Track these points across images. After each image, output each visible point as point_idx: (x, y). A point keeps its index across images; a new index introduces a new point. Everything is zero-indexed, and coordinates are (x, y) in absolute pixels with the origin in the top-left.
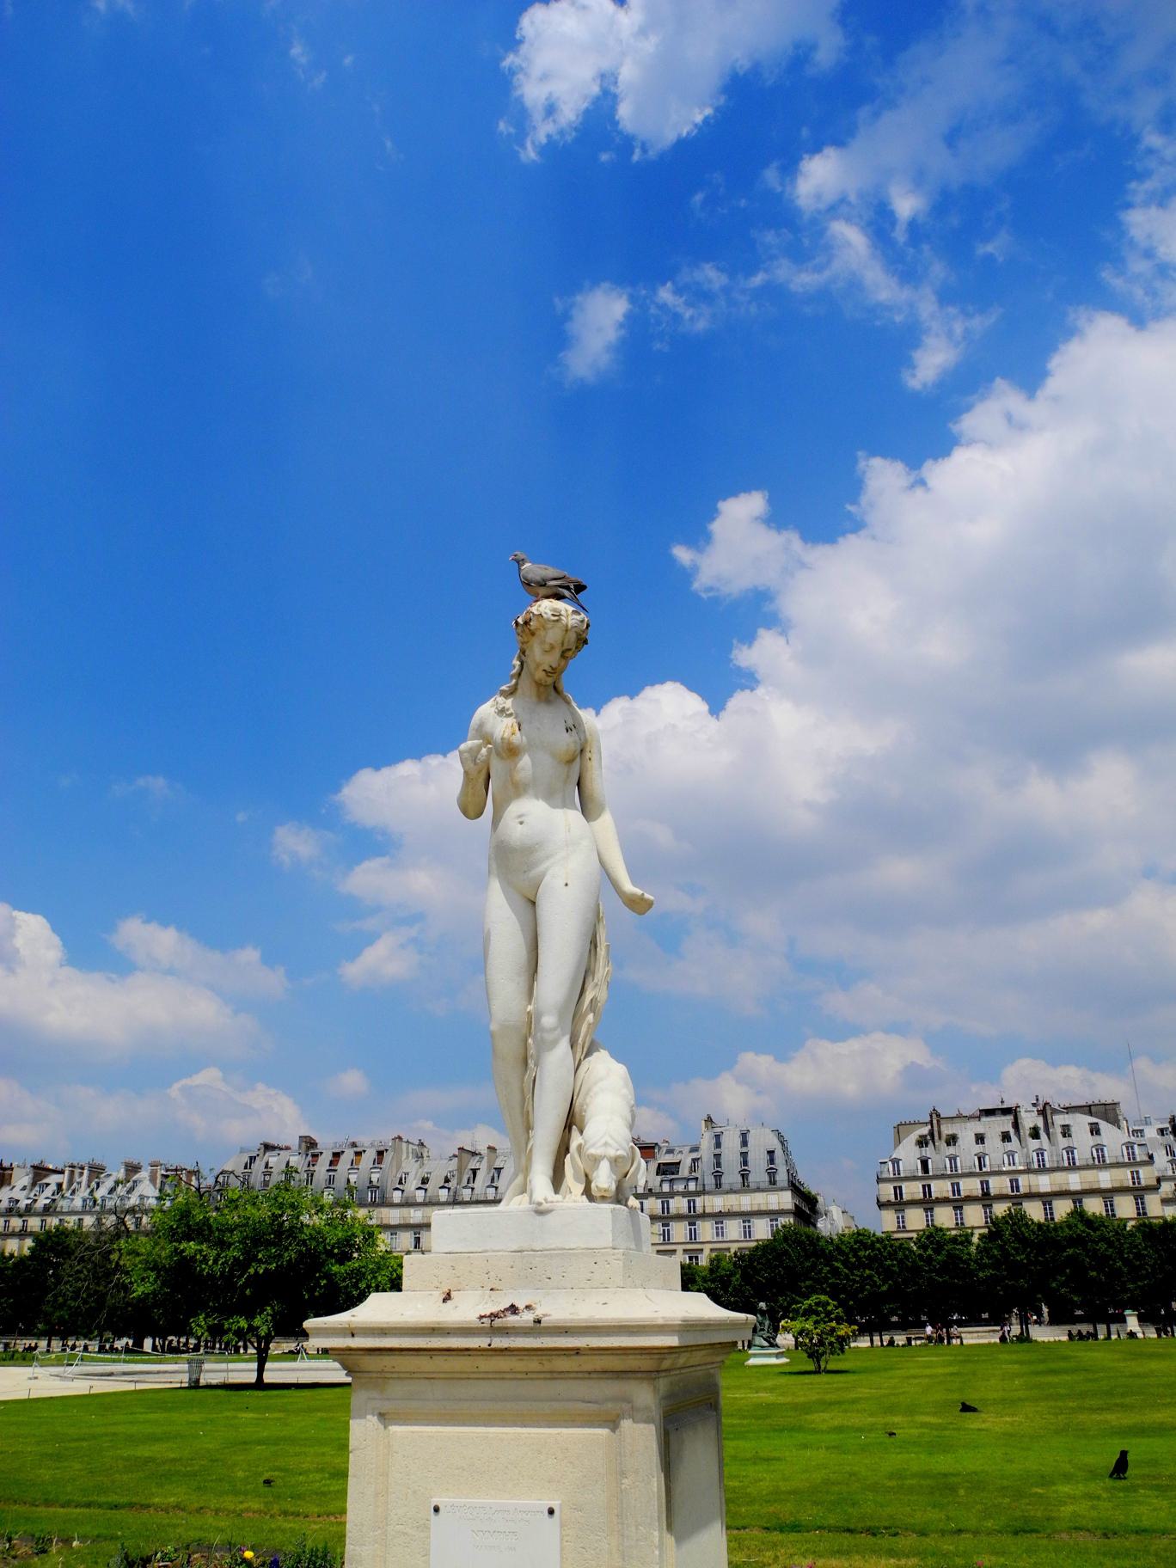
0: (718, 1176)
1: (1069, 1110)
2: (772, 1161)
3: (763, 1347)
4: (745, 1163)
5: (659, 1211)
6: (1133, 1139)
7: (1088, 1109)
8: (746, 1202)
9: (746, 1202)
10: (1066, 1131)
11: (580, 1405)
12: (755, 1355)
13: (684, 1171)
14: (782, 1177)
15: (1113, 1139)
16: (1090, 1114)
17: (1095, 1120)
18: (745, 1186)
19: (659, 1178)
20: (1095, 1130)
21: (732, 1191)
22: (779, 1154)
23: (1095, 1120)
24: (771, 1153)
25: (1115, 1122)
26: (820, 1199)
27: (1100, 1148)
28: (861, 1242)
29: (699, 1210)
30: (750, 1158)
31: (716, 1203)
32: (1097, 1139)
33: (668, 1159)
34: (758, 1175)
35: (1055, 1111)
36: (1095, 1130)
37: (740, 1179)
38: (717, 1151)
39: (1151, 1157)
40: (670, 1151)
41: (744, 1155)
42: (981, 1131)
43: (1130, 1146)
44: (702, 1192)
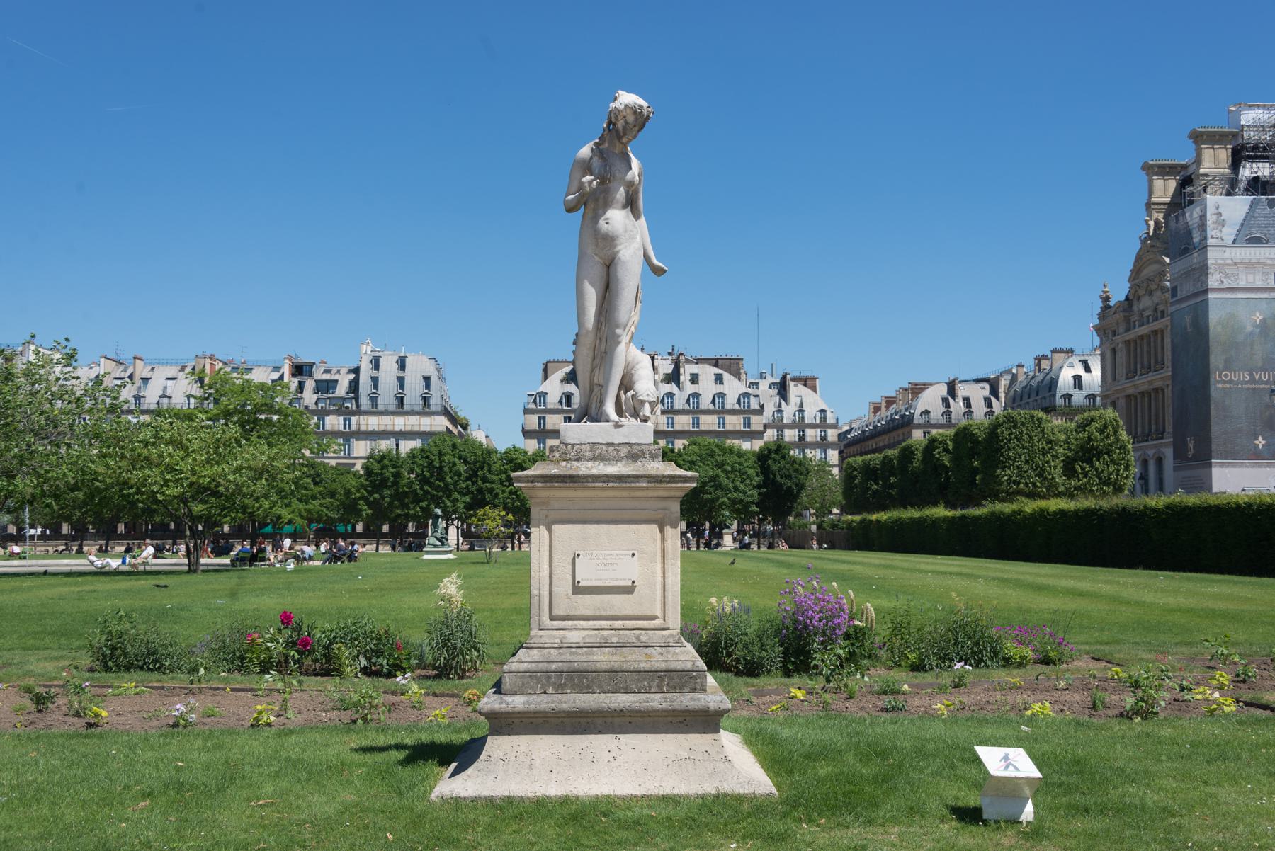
0: (374, 399)
1: (698, 361)
2: (428, 386)
3: (435, 546)
4: (402, 386)
5: (663, 427)
6: (749, 390)
7: (716, 363)
8: (400, 423)
9: (400, 423)
10: (694, 379)
11: (546, 593)
12: (428, 553)
13: (341, 390)
14: (435, 403)
15: (733, 388)
16: (716, 365)
17: (720, 371)
18: (375, 411)
19: (315, 396)
20: (719, 379)
21: (412, 413)
22: (434, 380)
23: (720, 371)
24: (427, 379)
25: (737, 374)
27: (722, 395)
28: (511, 461)
29: (353, 428)
30: (407, 381)
31: (372, 423)
32: (720, 389)
33: (326, 377)
34: (413, 400)
35: (688, 361)
36: (719, 379)
37: (422, 403)
38: (401, 373)
39: (762, 407)
40: (327, 371)
41: (401, 380)
42: (695, 371)
43: (747, 395)
44: (359, 412)
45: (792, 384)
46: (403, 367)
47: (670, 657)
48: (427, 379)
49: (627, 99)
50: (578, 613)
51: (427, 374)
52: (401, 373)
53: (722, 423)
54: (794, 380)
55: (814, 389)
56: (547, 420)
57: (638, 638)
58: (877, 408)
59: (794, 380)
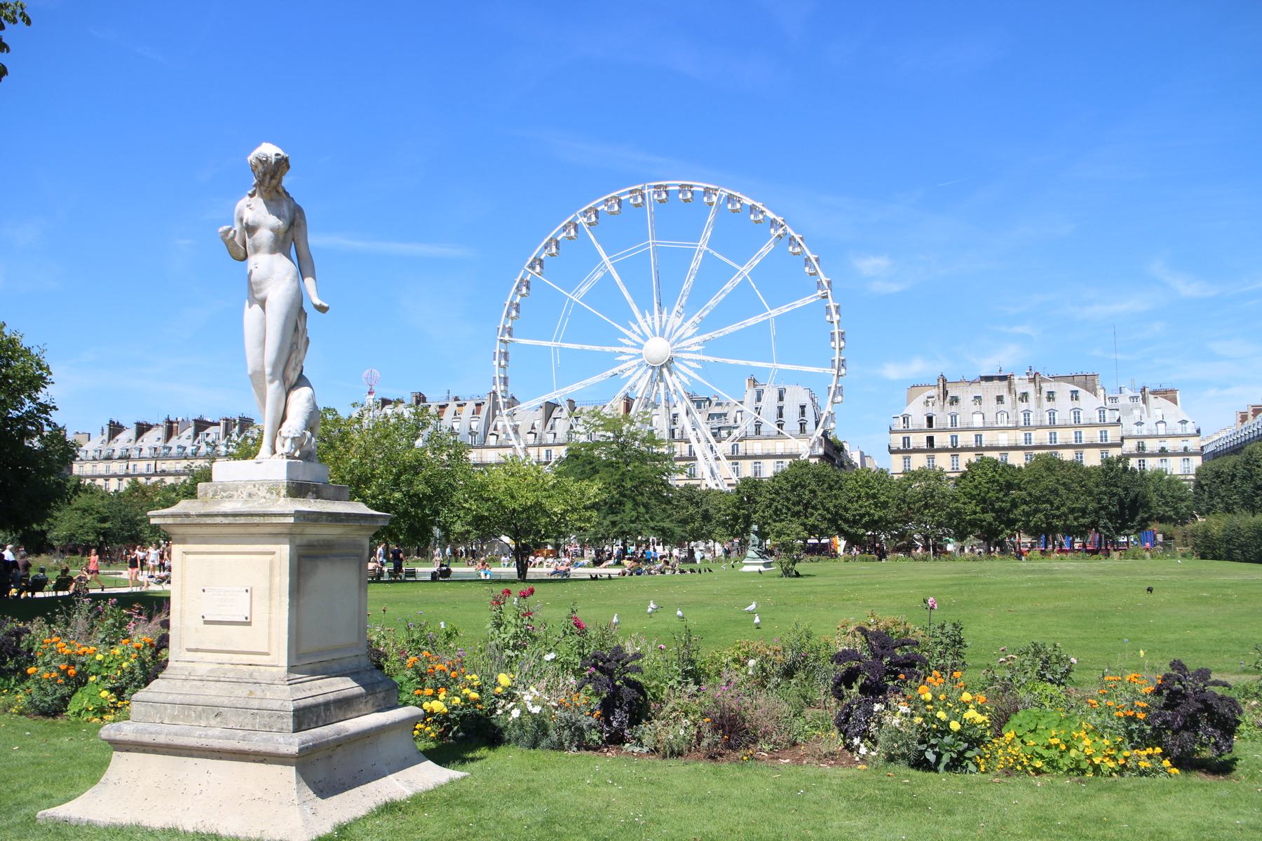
1: (1056, 378)
2: (803, 413)
7: (1070, 379)
15: (1089, 405)
16: (1073, 383)
17: (1076, 388)
21: (768, 438)
23: (1076, 388)
24: (803, 407)
25: (1094, 391)
26: (846, 446)
32: (1076, 404)
36: (1075, 395)
38: (781, 404)
45: (1151, 397)
46: (781, 399)
47: (268, 695)
48: (803, 407)
49: (269, 150)
50: (204, 647)
51: (803, 403)
52: (759, 404)
53: (1053, 437)
54: (1154, 393)
55: (1174, 401)
56: (1109, 434)
57: (251, 675)
58: (1244, 418)
59: (1154, 393)
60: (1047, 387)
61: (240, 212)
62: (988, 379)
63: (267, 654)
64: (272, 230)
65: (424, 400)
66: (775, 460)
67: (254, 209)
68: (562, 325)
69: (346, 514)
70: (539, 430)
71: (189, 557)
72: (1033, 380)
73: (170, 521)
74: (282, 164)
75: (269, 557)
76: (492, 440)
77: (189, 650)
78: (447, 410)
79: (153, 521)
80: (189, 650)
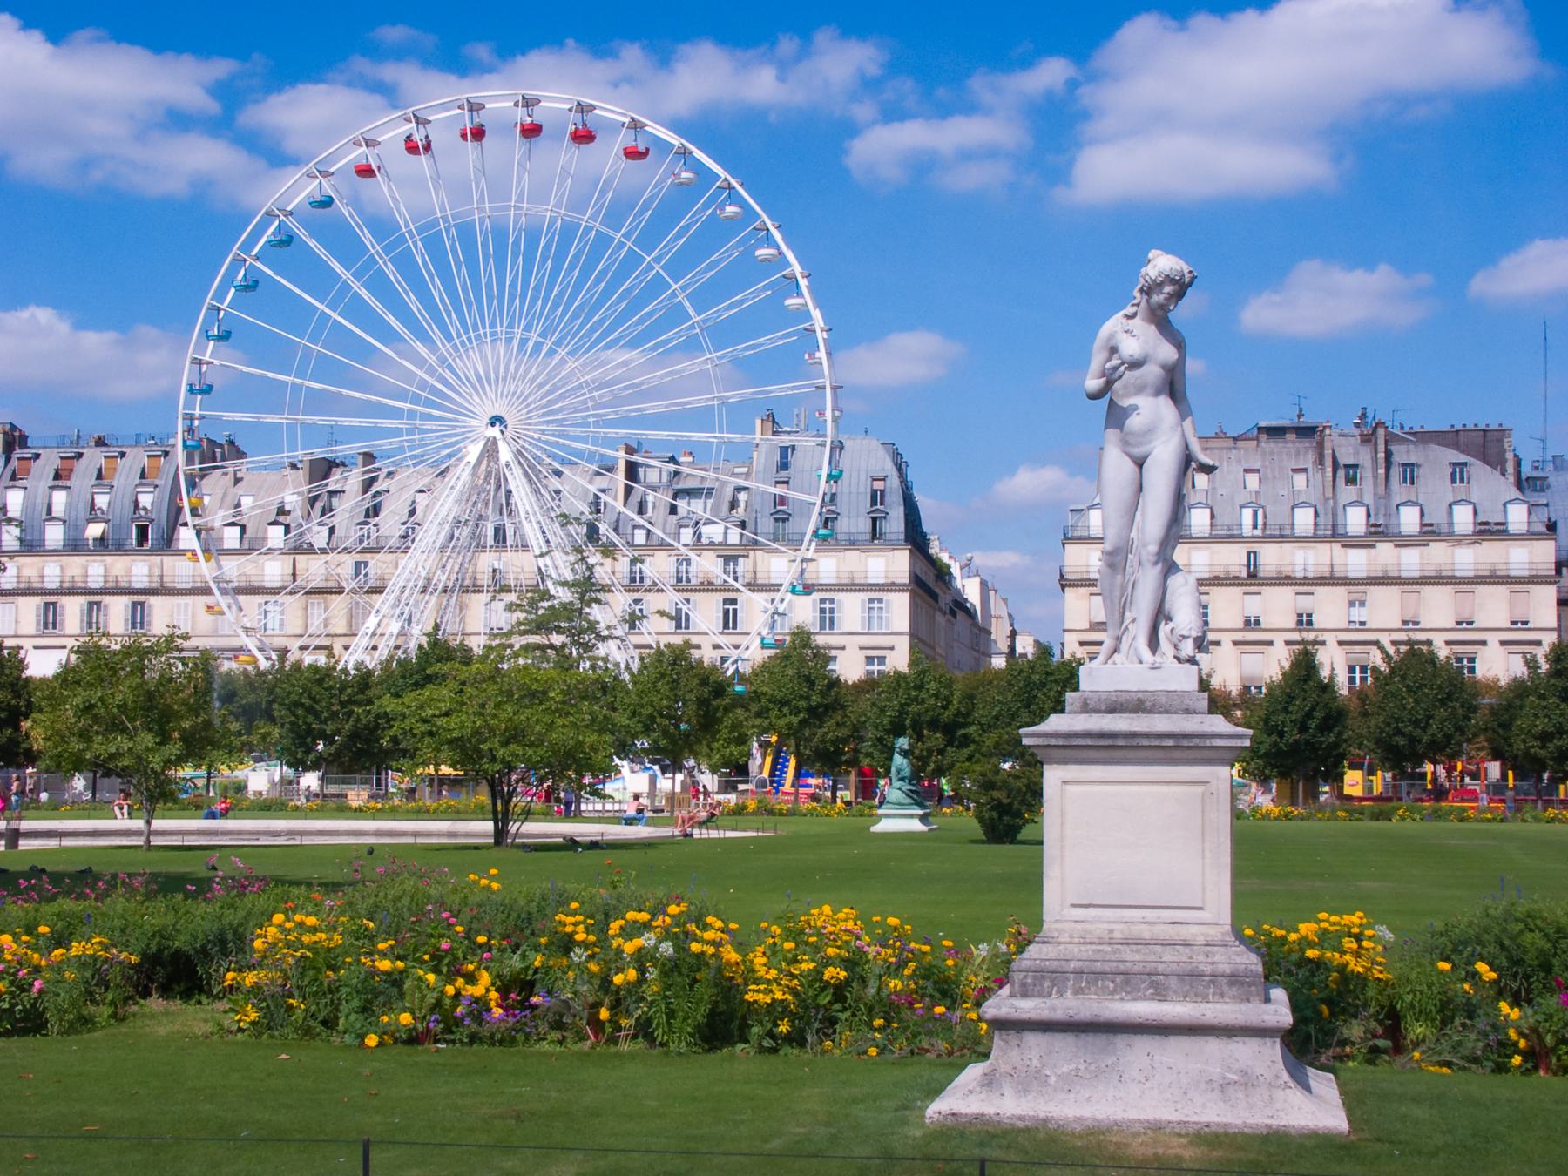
16: (1456, 446)
17: (1463, 458)
21: (852, 544)
23: (1463, 458)
60: (1401, 454)
61: (1112, 336)
62: (1275, 432)
63: (1201, 909)
64: (1164, 367)
65: (23, 441)
66: (865, 596)
67: (1132, 335)
68: (447, 310)
69: (1088, 735)
70: (296, 516)
71: (1071, 788)
72: (1367, 439)
73: (1039, 741)
74: (1181, 287)
75: (1200, 789)
76: (186, 537)
77: (1074, 906)
78: (80, 466)
79: (1025, 741)
80: (1074, 906)
